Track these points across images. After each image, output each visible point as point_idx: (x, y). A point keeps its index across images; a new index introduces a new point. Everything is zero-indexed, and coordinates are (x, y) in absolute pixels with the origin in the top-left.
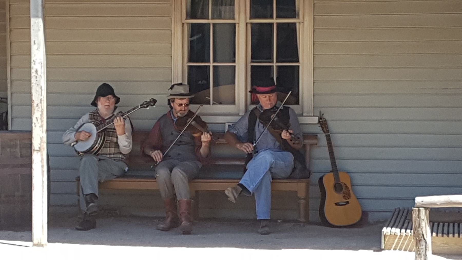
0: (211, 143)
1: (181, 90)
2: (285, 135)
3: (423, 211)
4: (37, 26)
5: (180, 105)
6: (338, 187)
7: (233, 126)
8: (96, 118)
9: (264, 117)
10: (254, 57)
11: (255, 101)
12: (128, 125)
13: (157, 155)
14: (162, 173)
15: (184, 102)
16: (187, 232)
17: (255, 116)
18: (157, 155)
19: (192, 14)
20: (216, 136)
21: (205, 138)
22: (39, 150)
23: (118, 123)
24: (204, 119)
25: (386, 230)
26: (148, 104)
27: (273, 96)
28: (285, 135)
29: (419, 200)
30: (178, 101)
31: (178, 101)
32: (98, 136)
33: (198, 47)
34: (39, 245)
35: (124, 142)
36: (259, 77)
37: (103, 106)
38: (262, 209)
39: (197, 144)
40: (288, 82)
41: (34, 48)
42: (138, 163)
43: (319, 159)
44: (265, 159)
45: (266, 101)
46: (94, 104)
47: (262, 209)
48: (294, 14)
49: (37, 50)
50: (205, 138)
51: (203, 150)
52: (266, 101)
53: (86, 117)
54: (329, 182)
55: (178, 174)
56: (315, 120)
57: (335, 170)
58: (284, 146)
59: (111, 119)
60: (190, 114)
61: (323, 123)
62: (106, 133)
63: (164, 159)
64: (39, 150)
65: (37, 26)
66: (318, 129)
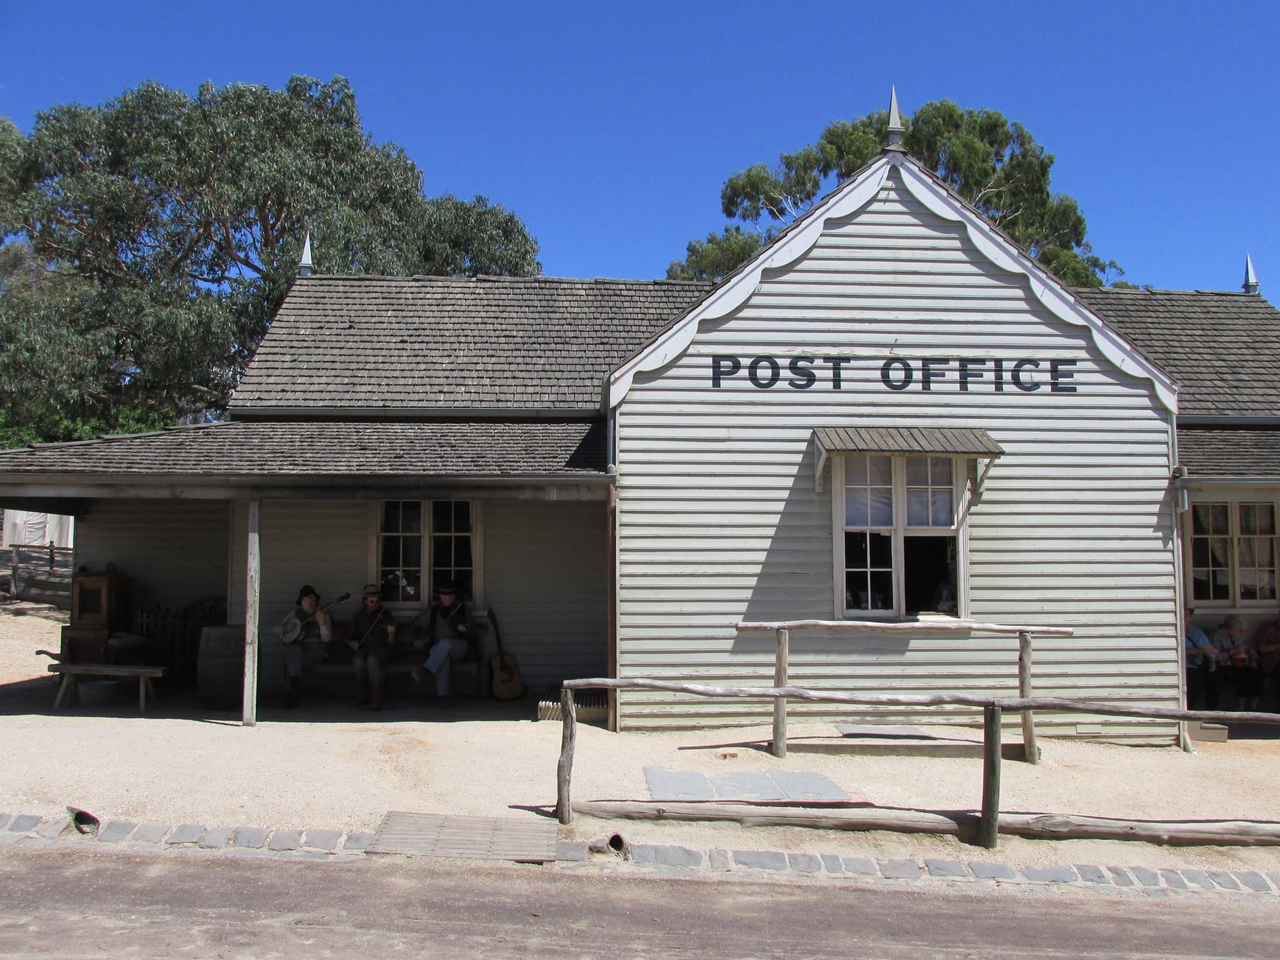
0: (396, 634)
1: (372, 590)
2: (461, 628)
3: (569, 692)
4: (254, 540)
5: (372, 601)
6: (504, 667)
7: (417, 618)
8: (300, 614)
9: (445, 611)
10: (436, 564)
11: (436, 598)
12: (328, 619)
13: (354, 645)
14: (358, 662)
15: (375, 599)
16: (379, 709)
17: (436, 610)
18: (354, 645)
19: (385, 528)
20: (402, 627)
21: (391, 629)
22: (252, 643)
23: (320, 617)
24: (394, 613)
25: (542, 704)
26: (343, 598)
27: (453, 597)
28: (461, 628)
29: (566, 682)
30: (370, 599)
31: (370, 599)
32: (303, 628)
33: (390, 555)
34: (249, 724)
35: (325, 632)
36: (440, 580)
37: (306, 604)
38: (442, 687)
39: (385, 634)
40: (462, 585)
41: (250, 558)
42: (337, 650)
43: (489, 641)
44: (444, 647)
45: (446, 600)
46: (299, 603)
47: (442, 687)
48: (469, 529)
49: (591, 849)
50: (391, 629)
51: (391, 639)
52: (446, 600)
53: (292, 614)
54: (496, 663)
55: (372, 660)
56: (485, 613)
57: (501, 652)
58: (460, 636)
59: (314, 613)
60: (380, 608)
61: (492, 616)
62: (310, 626)
63: (361, 647)
64: (252, 643)
65: (254, 540)
66: (487, 621)
